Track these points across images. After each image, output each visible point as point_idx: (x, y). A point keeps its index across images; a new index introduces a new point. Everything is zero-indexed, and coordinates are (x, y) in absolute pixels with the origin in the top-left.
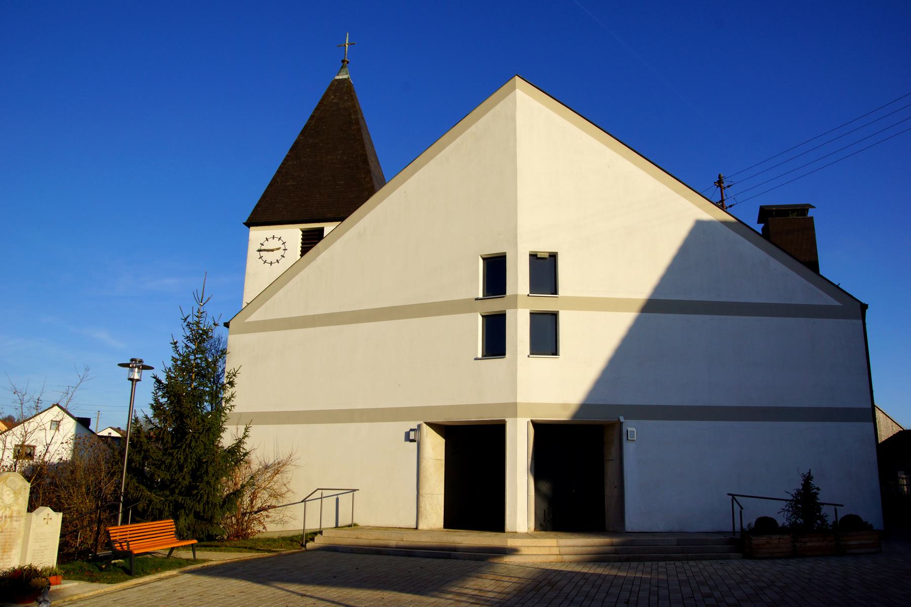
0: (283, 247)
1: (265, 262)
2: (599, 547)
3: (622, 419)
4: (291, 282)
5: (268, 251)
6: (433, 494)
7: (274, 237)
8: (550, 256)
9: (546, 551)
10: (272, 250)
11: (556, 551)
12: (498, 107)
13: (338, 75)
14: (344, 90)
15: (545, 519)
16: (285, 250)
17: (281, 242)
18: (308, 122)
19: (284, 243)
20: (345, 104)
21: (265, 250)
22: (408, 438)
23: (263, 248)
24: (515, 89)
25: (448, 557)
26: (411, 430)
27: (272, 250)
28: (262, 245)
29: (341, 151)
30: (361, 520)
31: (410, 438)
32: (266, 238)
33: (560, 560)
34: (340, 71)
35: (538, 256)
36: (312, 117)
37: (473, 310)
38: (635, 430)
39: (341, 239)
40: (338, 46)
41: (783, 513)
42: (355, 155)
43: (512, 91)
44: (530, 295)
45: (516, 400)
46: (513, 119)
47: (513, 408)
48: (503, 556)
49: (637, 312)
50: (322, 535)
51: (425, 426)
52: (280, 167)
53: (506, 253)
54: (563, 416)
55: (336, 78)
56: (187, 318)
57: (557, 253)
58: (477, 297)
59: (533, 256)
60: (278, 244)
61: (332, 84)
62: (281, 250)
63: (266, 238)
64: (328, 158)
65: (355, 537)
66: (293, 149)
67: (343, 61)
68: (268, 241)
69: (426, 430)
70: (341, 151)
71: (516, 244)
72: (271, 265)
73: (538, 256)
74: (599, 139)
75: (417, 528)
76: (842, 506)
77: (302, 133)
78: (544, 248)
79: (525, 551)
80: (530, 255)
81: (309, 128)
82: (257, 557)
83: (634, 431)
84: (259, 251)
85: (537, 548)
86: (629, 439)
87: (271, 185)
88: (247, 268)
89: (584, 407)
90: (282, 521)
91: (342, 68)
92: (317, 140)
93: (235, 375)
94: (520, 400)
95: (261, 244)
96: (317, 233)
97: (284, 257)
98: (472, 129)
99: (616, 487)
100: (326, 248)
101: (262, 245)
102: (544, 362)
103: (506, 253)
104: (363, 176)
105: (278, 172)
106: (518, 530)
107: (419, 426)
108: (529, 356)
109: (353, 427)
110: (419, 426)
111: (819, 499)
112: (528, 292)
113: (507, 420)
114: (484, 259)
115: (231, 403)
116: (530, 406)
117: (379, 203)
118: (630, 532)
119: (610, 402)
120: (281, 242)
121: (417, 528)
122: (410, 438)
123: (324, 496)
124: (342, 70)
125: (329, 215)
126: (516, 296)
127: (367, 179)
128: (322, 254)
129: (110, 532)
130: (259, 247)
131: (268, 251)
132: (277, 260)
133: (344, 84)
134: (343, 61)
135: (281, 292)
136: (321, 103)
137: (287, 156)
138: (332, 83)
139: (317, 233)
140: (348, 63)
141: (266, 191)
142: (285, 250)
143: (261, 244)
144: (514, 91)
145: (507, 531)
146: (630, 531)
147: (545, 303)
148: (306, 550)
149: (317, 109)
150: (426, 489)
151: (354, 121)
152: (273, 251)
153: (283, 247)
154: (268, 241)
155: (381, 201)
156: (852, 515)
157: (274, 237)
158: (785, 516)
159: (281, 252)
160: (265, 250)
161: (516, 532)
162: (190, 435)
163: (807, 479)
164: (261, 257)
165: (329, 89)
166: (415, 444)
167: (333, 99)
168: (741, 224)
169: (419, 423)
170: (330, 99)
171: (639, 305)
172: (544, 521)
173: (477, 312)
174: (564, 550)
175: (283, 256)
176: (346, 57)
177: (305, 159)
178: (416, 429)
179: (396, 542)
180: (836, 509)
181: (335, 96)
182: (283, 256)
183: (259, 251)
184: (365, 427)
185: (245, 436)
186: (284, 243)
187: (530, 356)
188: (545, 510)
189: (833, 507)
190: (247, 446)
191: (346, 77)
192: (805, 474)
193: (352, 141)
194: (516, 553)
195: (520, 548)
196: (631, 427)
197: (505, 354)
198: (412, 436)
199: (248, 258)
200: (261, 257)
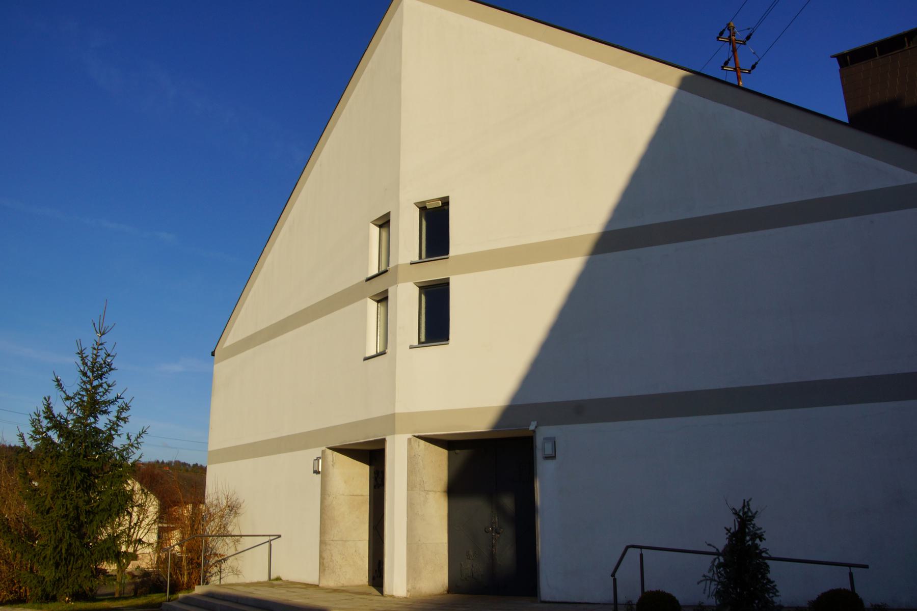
6: (346, 541)
35: (428, 208)
41: (704, 582)
49: (587, 255)
51: (330, 452)
54: (481, 425)
74: (506, 26)
76: (866, 567)
89: (510, 412)
90: (236, 572)
106: (395, 594)
110: (323, 452)
116: (411, 416)
118: (549, 602)
123: (268, 543)
146: (548, 599)
156: (833, 589)
158: (707, 592)
163: (745, 518)
168: (700, 78)
169: (324, 448)
171: (587, 246)
173: (364, 297)
180: (851, 575)
189: (846, 570)
192: (239, 545)
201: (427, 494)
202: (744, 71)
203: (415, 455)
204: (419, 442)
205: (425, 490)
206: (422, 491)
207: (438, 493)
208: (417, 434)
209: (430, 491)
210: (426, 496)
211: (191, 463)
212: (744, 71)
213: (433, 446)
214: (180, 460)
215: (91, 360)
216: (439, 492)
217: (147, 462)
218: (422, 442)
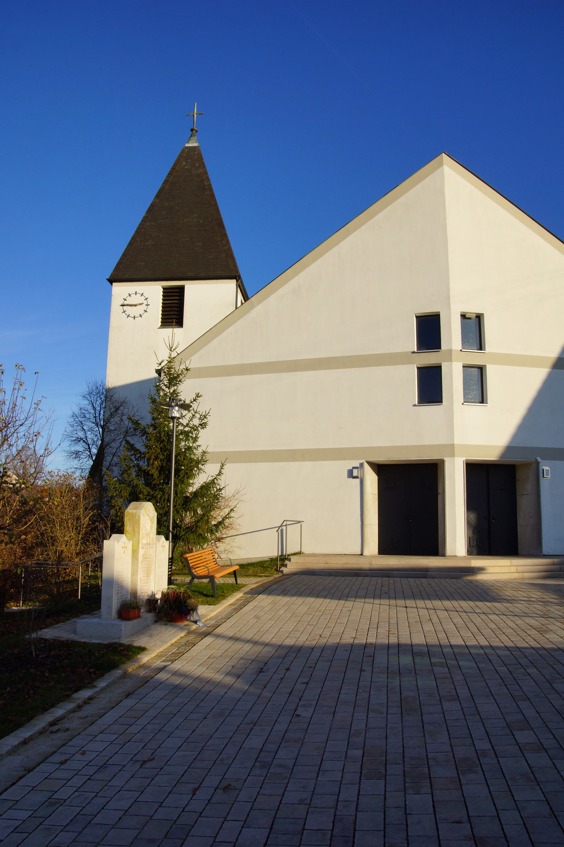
0: (145, 302)
1: (128, 316)
2: (548, 566)
3: (539, 459)
4: (225, 332)
5: (131, 305)
7: (136, 293)
8: (476, 317)
9: (506, 570)
10: (135, 305)
11: (513, 569)
12: (427, 180)
13: (188, 143)
14: (195, 157)
15: (470, 544)
16: (148, 305)
17: (143, 298)
18: (162, 186)
19: (146, 299)
20: (197, 170)
21: (128, 305)
22: (350, 474)
23: (126, 303)
24: (443, 165)
25: (425, 577)
26: (354, 468)
27: (135, 305)
28: (125, 300)
29: (197, 215)
30: (306, 550)
31: (354, 475)
32: (129, 294)
33: (522, 577)
34: (190, 139)
36: (166, 182)
37: (409, 362)
38: (549, 469)
39: (275, 294)
40: (186, 115)
42: (210, 219)
43: (437, 169)
44: (463, 350)
45: (454, 442)
46: (442, 193)
47: (451, 449)
48: (476, 574)
50: (290, 561)
52: (138, 228)
53: (439, 312)
55: (186, 146)
56: (161, 363)
57: (483, 314)
58: (413, 351)
59: (463, 316)
60: (140, 300)
61: (183, 151)
62: (144, 305)
63: (129, 294)
64: (185, 220)
65: (324, 562)
66: (149, 211)
67: (192, 130)
68: (130, 296)
69: (367, 468)
70: (197, 215)
71: (449, 305)
72: (134, 319)
73: (467, 316)
75: (362, 555)
77: (158, 196)
78: (472, 309)
79: (490, 570)
80: (461, 315)
81: (164, 191)
82: (267, 581)
83: (549, 470)
84: (123, 305)
85: (499, 567)
86: (545, 476)
87: (130, 244)
88: (111, 321)
89: (509, 449)
91: (191, 136)
92: (173, 204)
93: (205, 417)
94: (456, 442)
95: (124, 299)
96: (177, 290)
97: (147, 312)
98: (403, 199)
99: (531, 517)
100: (260, 302)
101: (125, 300)
102: (477, 408)
103: (439, 312)
104: (220, 239)
105: (137, 232)
107: (362, 465)
108: (463, 404)
109: (294, 466)
110: (362, 465)
111: (118, 543)
112: (460, 348)
113: (445, 459)
114: (417, 317)
115: (198, 443)
117: (313, 262)
119: (529, 445)
120: (143, 298)
121: (362, 555)
122: (354, 475)
124: (192, 138)
125: (189, 274)
126: (450, 351)
127: (224, 242)
128: (256, 308)
129: (189, 559)
130: (122, 302)
131: (131, 305)
132: (140, 315)
133: (195, 151)
134: (192, 130)
135: (215, 341)
136: (173, 169)
137: (144, 217)
138: (182, 150)
139: (177, 290)
140: (196, 131)
141: (127, 250)
142: (148, 305)
143: (124, 299)
144: (442, 167)
145: (448, 555)
147: (475, 358)
148: (284, 575)
149: (170, 174)
150: (366, 522)
151: (206, 187)
152: (136, 306)
153: (145, 302)
154: (130, 296)
155: (315, 260)
157: (136, 293)
159: (144, 307)
160: (128, 305)
161: (456, 556)
162: (183, 471)
164: (124, 312)
165: (180, 156)
166: (358, 481)
167: (185, 165)
169: (361, 461)
170: (182, 165)
171: (550, 363)
172: (470, 547)
173: (415, 364)
174: (520, 569)
175: (145, 311)
176: (195, 126)
177: (163, 221)
178: (358, 467)
179: (369, 565)
181: (187, 163)
182: (145, 311)
183: (123, 305)
184: (308, 466)
185: (220, 474)
186: (146, 299)
187: (464, 404)
188: (470, 537)
190: (221, 482)
191: (196, 145)
193: (206, 206)
194: (482, 572)
195: (485, 568)
196: (545, 467)
197: (441, 402)
198: (355, 473)
199: (111, 312)
200: (124, 312)
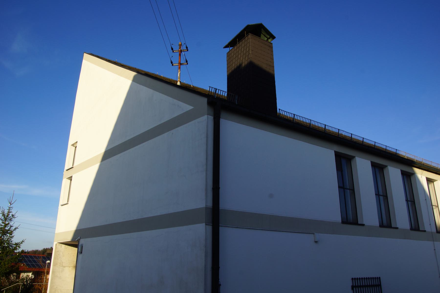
173: (333, 150)
201: (64, 268)
202: (183, 64)
203: (58, 251)
204: (61, 246)
205: (63, 266)
206: (61, 266)
207: (72, 267)
208: (59, 242)
209: (66, 266)
210: (63, 268)
211: (220, 266)
212: (183, 64)
213: (71, 247)
214: (34, 250)
215: (3, 218)
216: (72, 267)
217: (35, 250)
218: (63, 246)
